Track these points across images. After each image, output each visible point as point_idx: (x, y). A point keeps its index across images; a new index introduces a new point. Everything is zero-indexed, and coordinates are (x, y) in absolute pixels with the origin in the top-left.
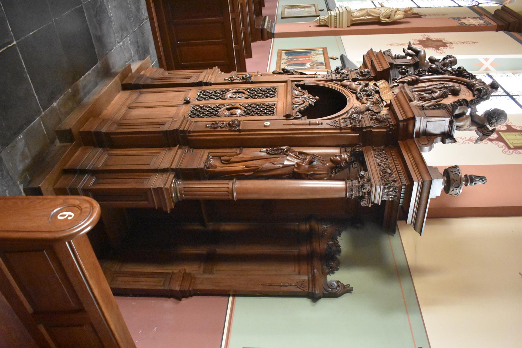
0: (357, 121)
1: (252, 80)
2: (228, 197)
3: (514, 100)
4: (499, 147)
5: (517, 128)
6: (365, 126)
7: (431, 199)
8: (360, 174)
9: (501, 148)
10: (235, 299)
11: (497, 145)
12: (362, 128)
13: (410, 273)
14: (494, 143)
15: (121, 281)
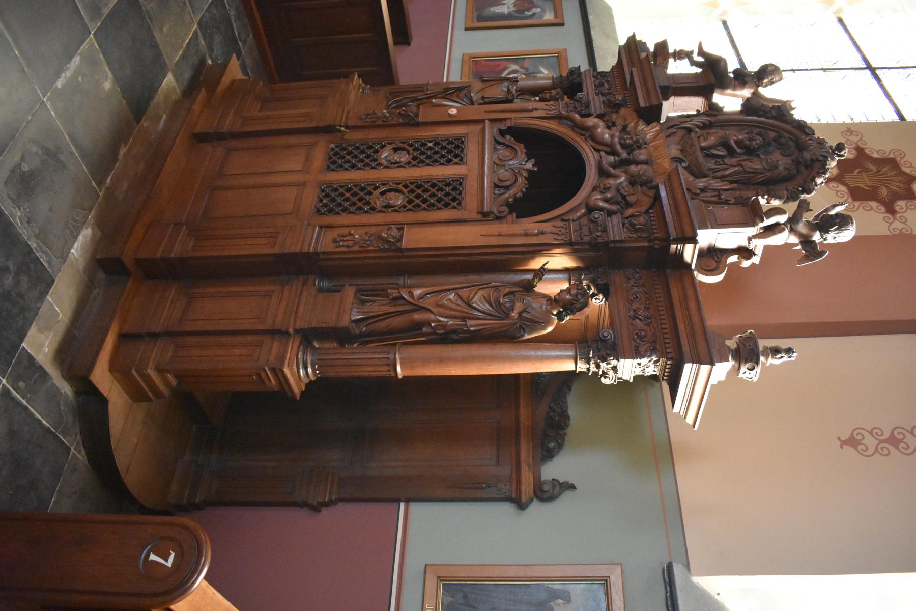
0: (599, 227)
1: (420, 119)
2: (389, 373)
3: (865, 60)
4: (837, 195)
5: (873, 153)
6: (612, 239)
7: (713, 386)
8: (601, 335)
9: (841, 197)
10: (409, 506)
11: (834, 192)
12: (606, 244)
13: (673, 463)
14: (831, 187)
15: (269, 227)
